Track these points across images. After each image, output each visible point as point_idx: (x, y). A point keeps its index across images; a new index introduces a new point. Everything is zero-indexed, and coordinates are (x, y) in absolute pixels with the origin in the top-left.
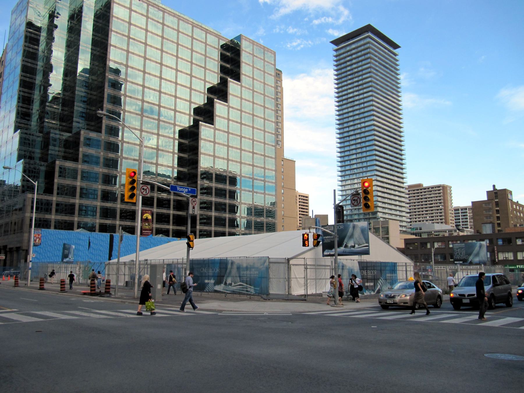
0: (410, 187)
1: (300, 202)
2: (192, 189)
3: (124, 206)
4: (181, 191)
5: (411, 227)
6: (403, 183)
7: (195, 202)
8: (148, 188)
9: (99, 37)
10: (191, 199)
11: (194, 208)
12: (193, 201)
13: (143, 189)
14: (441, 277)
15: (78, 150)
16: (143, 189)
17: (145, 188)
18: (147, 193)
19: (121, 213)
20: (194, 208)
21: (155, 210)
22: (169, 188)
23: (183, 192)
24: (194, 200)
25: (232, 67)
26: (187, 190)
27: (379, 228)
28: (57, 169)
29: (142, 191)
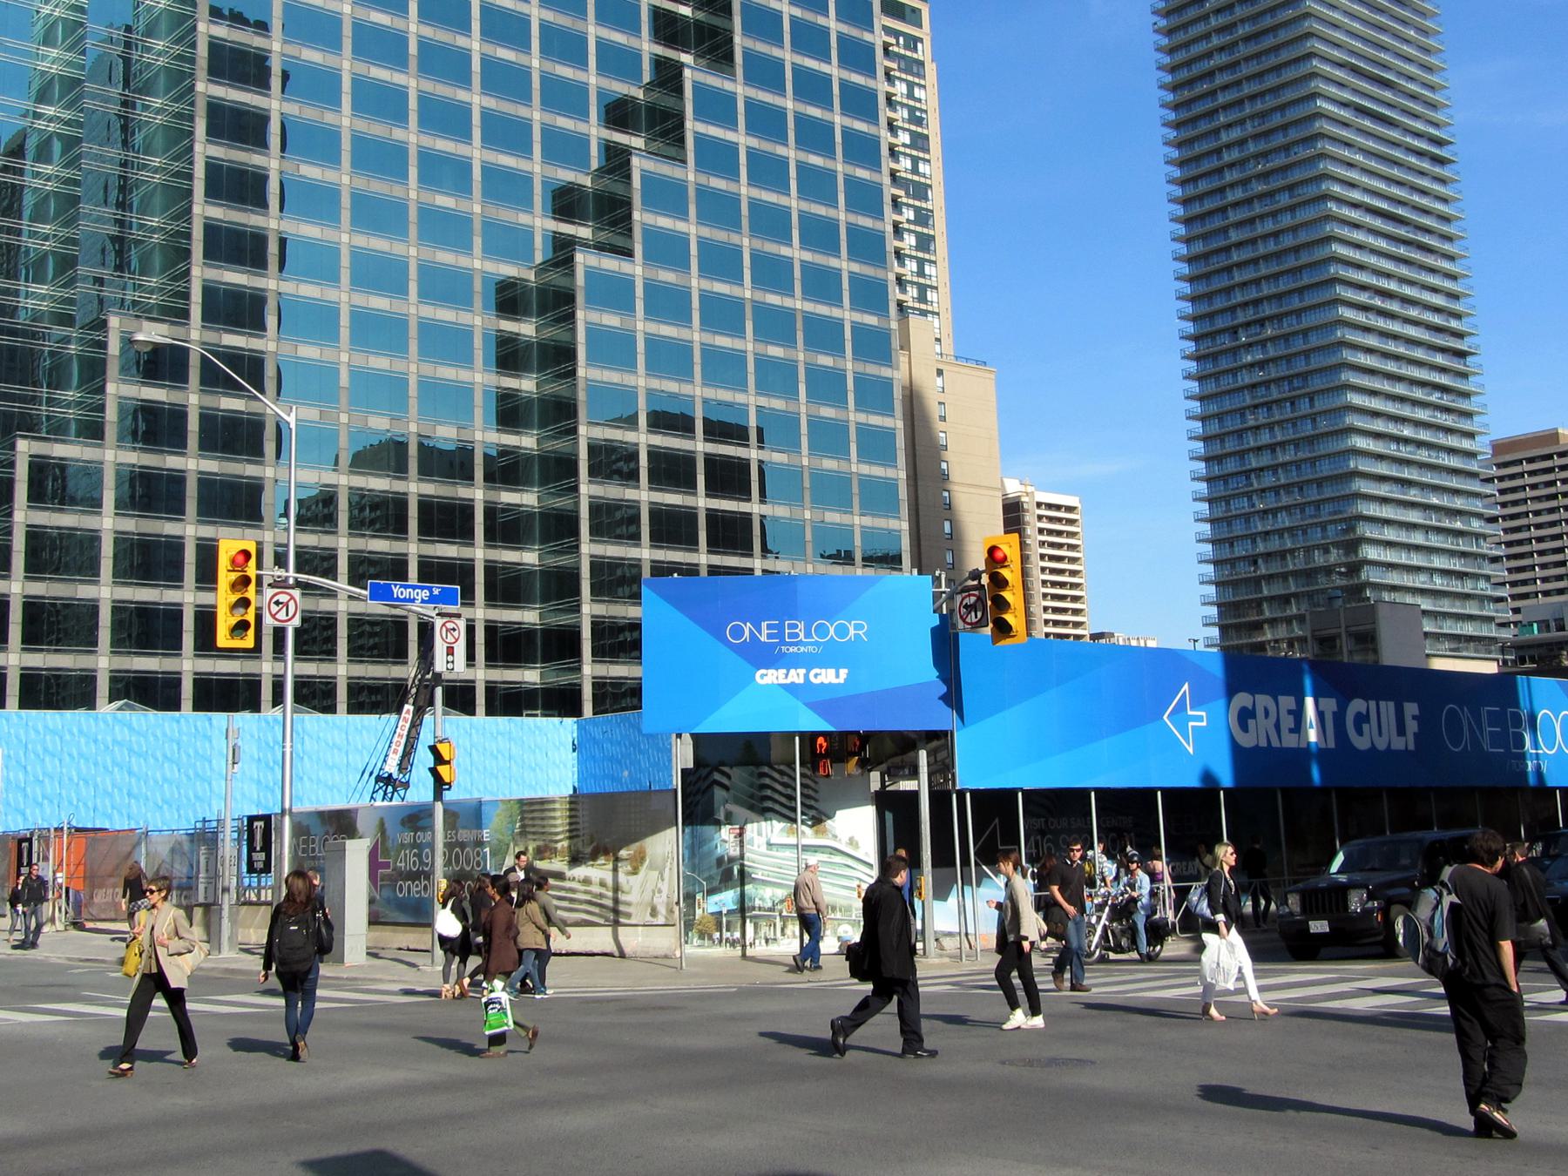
0: (1499, 447)
1: (1042, 544)
2: (443, 590)
3: (209, 665)
4: (405, 600)
5: (1518, 617)
6: (1471, 435)
7: (456, 634)
8: (292, 598)
9: (43, 298)
10: (439, 622)
11: (450, 651)
12: (447, 630)
13: (277, 603)
14: (562, 832)
15: (101, 390)
16: (277, 603)
17: (283, 598)
18: (291, 614)
19: (332, 639)
20: (450, 651)
21: (481, 613)
22: (364, 592)
23: (413, 600)
24: (450, 625)
25: (700, 16)
26: (425, 594)
27: (1339, 635)
28: (21, 473)
29: (274, 608)
